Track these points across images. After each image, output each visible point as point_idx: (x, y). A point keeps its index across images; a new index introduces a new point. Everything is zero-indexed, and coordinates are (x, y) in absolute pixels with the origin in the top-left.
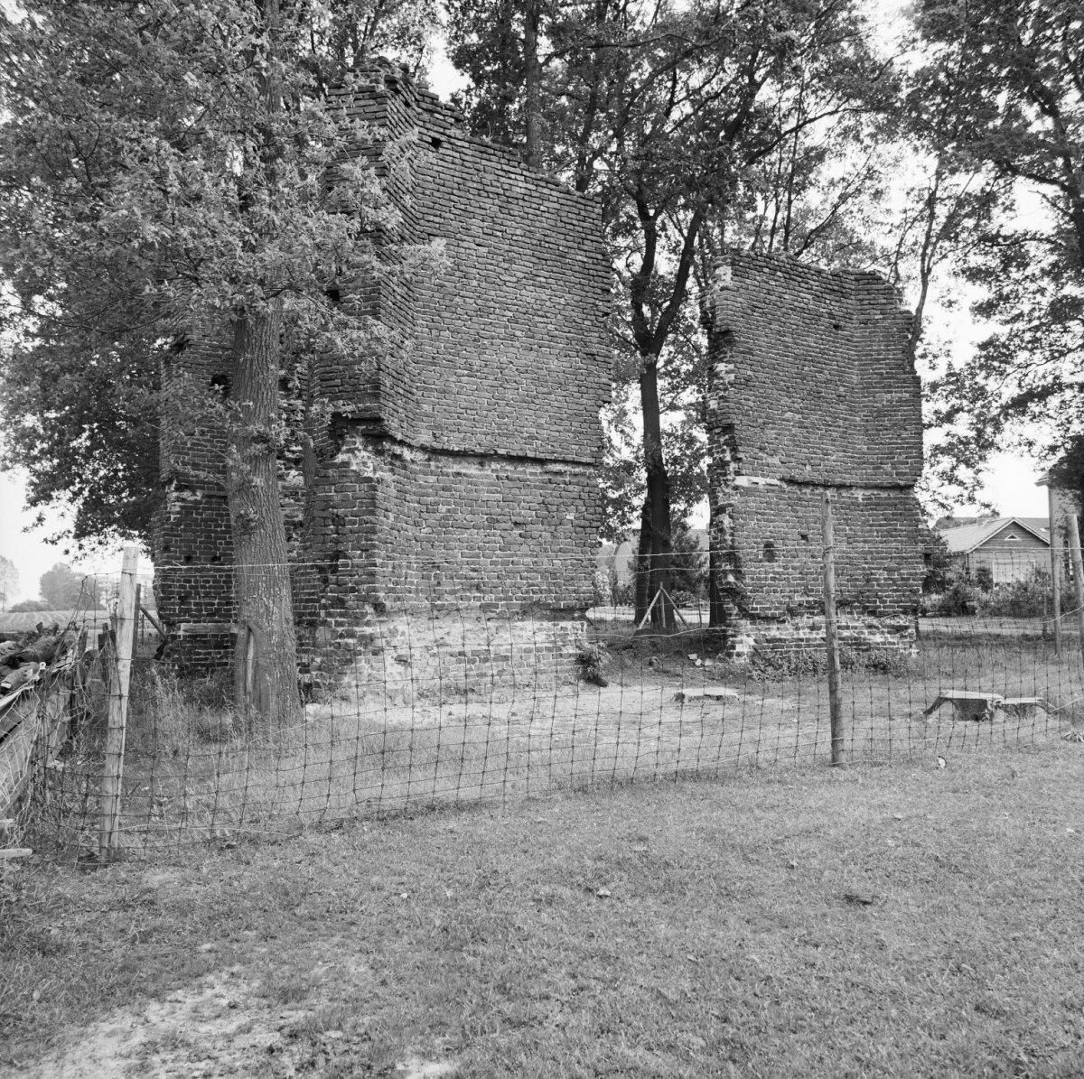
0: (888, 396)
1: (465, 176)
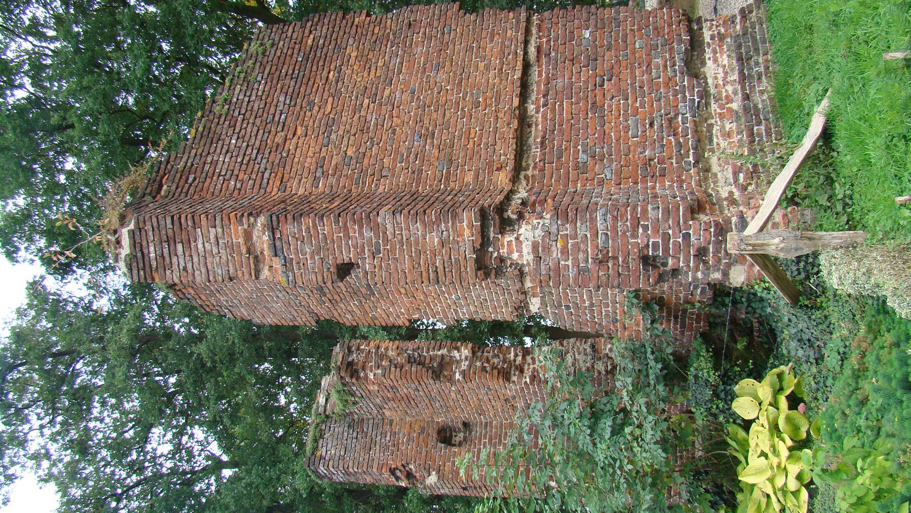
1: (224, 151)
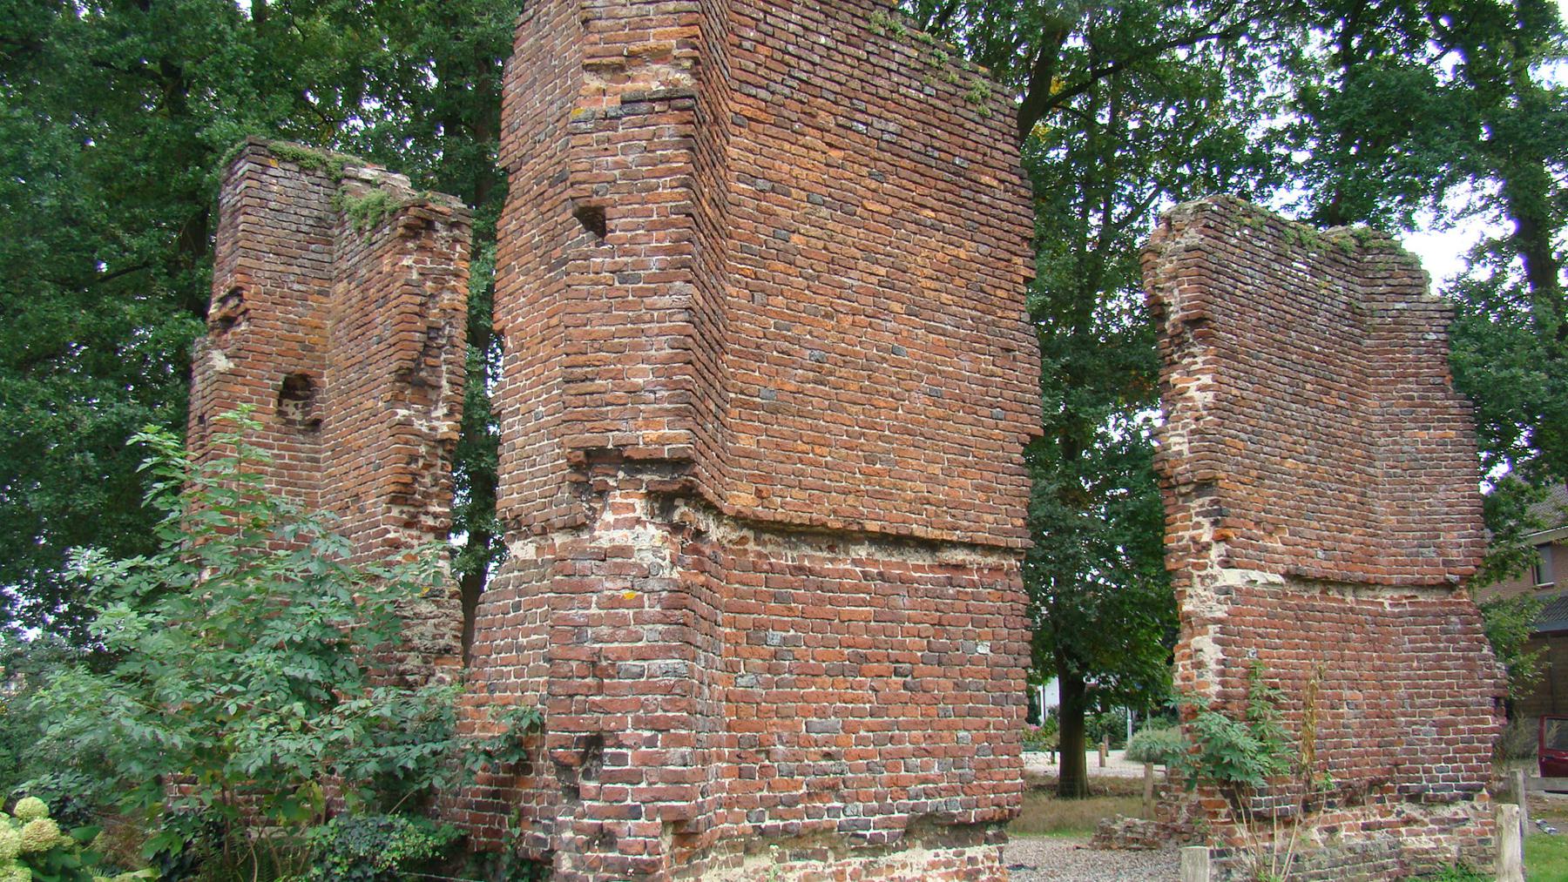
0: (1425, 435)
1: (807, 23)
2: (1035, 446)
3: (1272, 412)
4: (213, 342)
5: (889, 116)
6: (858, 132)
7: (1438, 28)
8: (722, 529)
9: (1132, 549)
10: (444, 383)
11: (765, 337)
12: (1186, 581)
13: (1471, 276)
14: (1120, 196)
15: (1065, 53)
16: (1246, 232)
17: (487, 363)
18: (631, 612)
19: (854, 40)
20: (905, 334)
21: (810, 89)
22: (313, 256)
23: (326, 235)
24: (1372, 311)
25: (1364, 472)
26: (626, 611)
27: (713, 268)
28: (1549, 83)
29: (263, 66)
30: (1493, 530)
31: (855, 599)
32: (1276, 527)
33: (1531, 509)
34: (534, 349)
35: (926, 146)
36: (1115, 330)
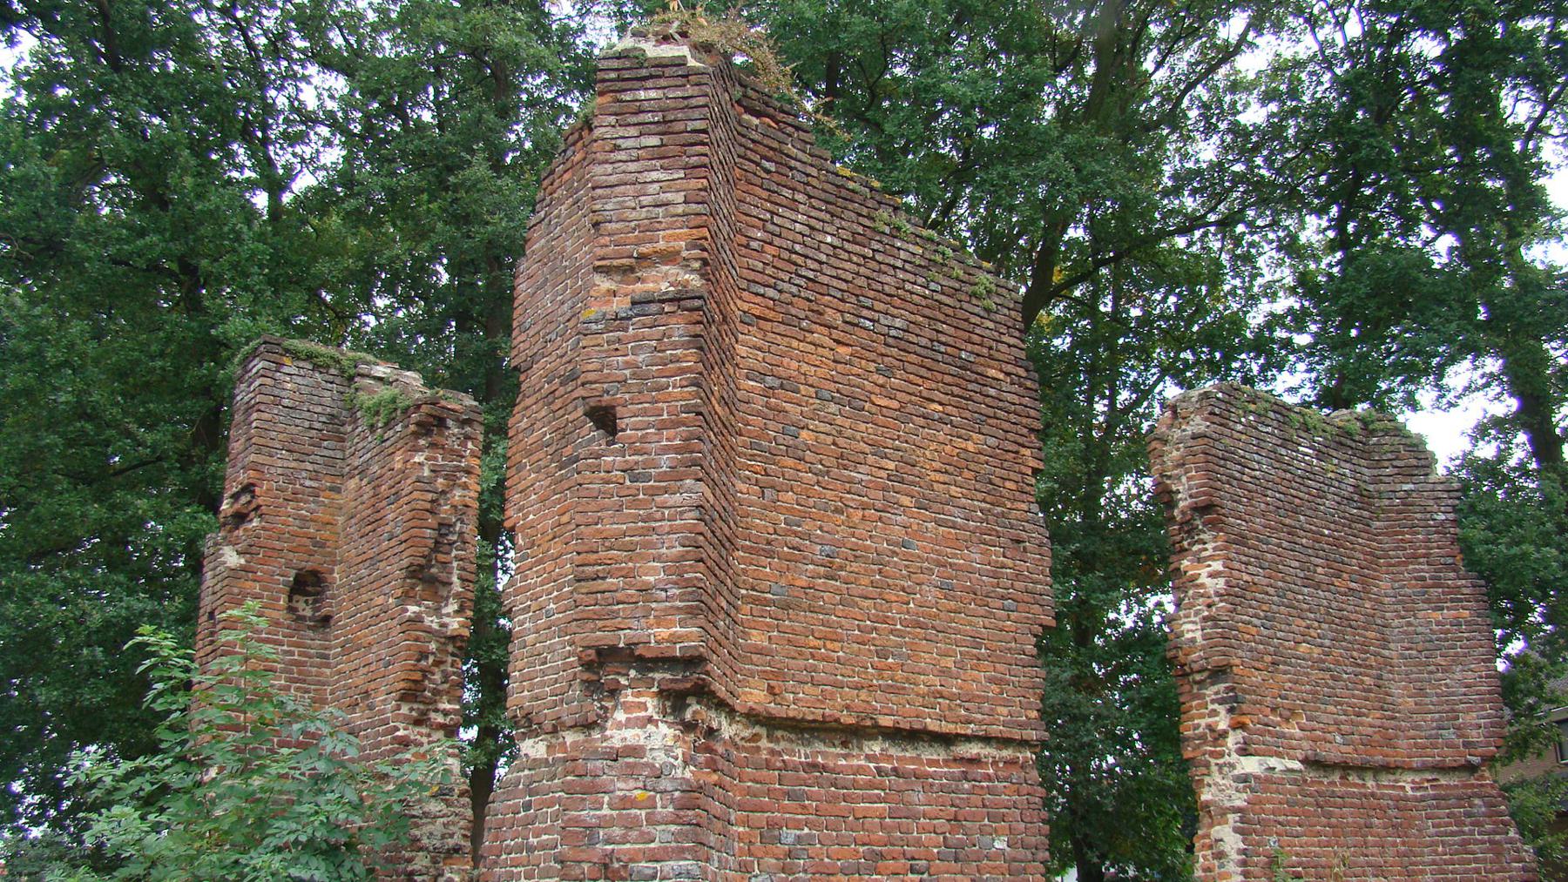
0: (1438, 615)
1: (813, 222)
2: (1048, 646)
3: (1284, 596)
4: (224, 538)
5: (895, 311)
6: (865, 328)
7: (1431, 211)
8: (734, 726)
9: (1148, 735)
10: (455, 579)
11: (775, 533)
12: (1203, 770)
13: (1476, 453)
14: (1125, 382)
15: (1067, 243)
16: (1251, 418)
17: (498, 557)
18: (643, 813)
19: (859, 238)
20: (915, 527)
21: (818, 287)
22: (326, 453)
23: (338, 431)
24: (1379, 492)
25: (1379, 654)
26: (638, 812)
27: (724, 466)
28: (1543, 262)
29: (278, 264)
30: (1513, 709)
31: (870, 796)
32: (1292, 711)
33: (1550, 685)
34: (545, 546)
35: (932, 341)
36: (1123, 515)
